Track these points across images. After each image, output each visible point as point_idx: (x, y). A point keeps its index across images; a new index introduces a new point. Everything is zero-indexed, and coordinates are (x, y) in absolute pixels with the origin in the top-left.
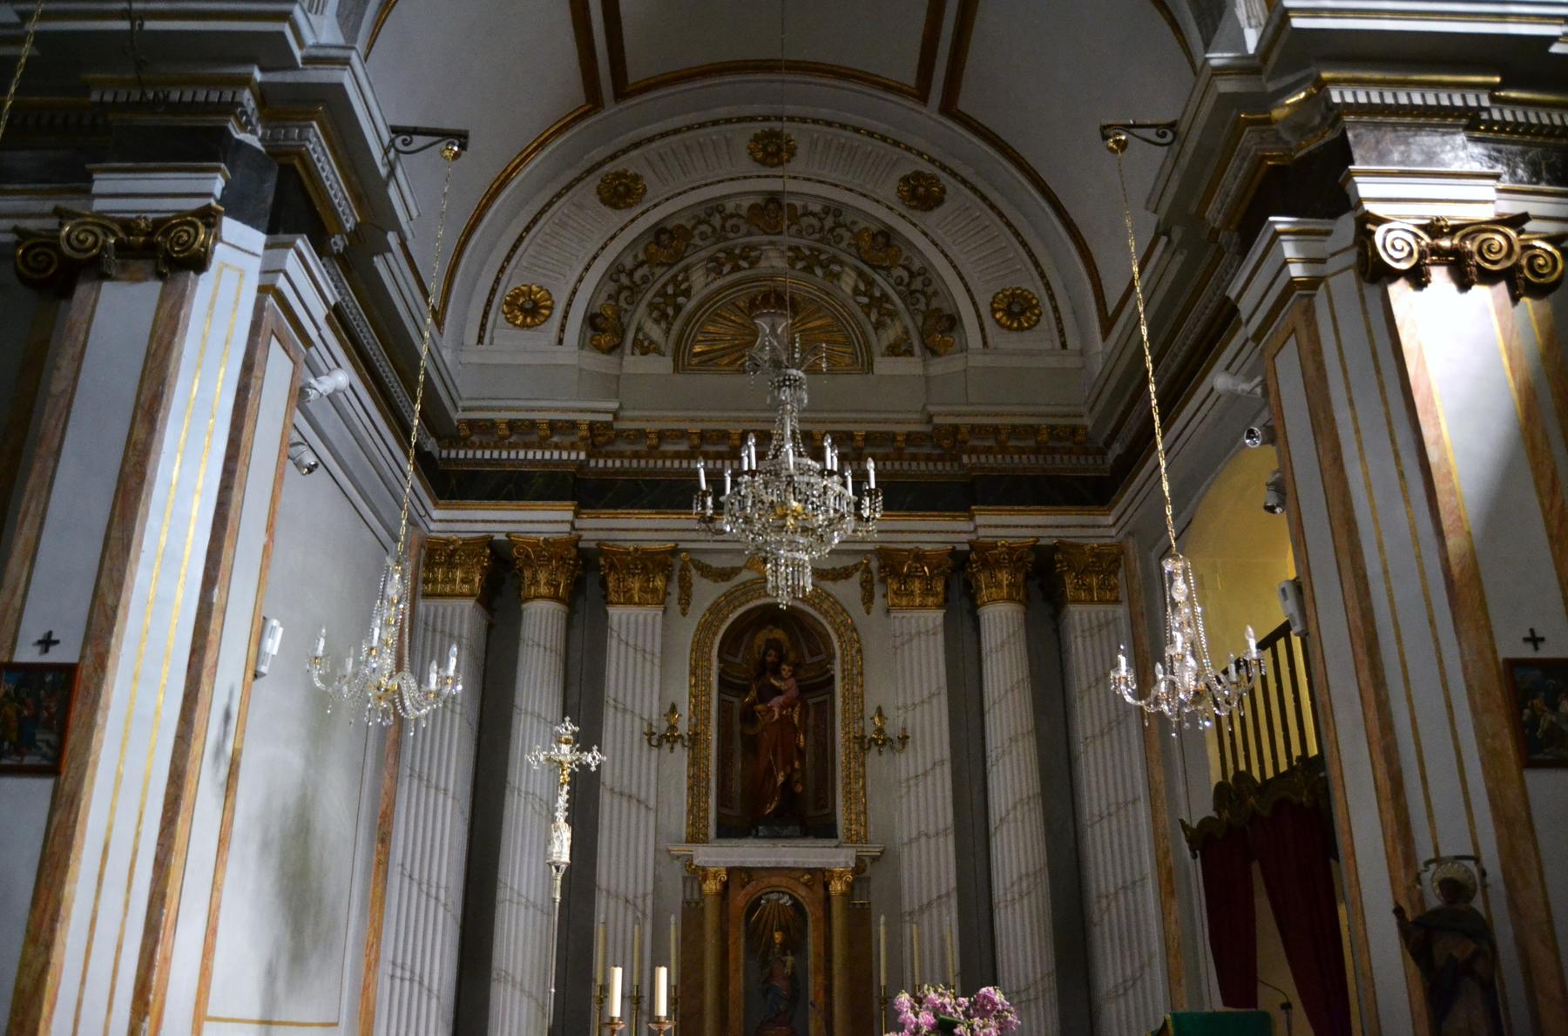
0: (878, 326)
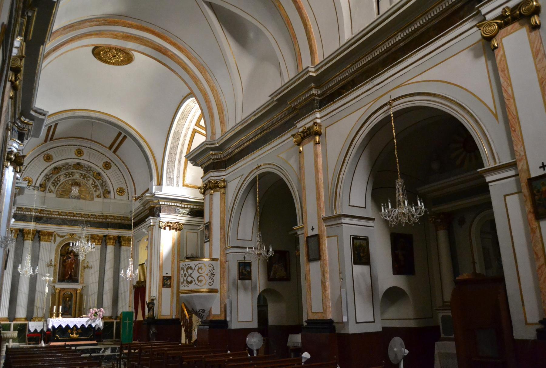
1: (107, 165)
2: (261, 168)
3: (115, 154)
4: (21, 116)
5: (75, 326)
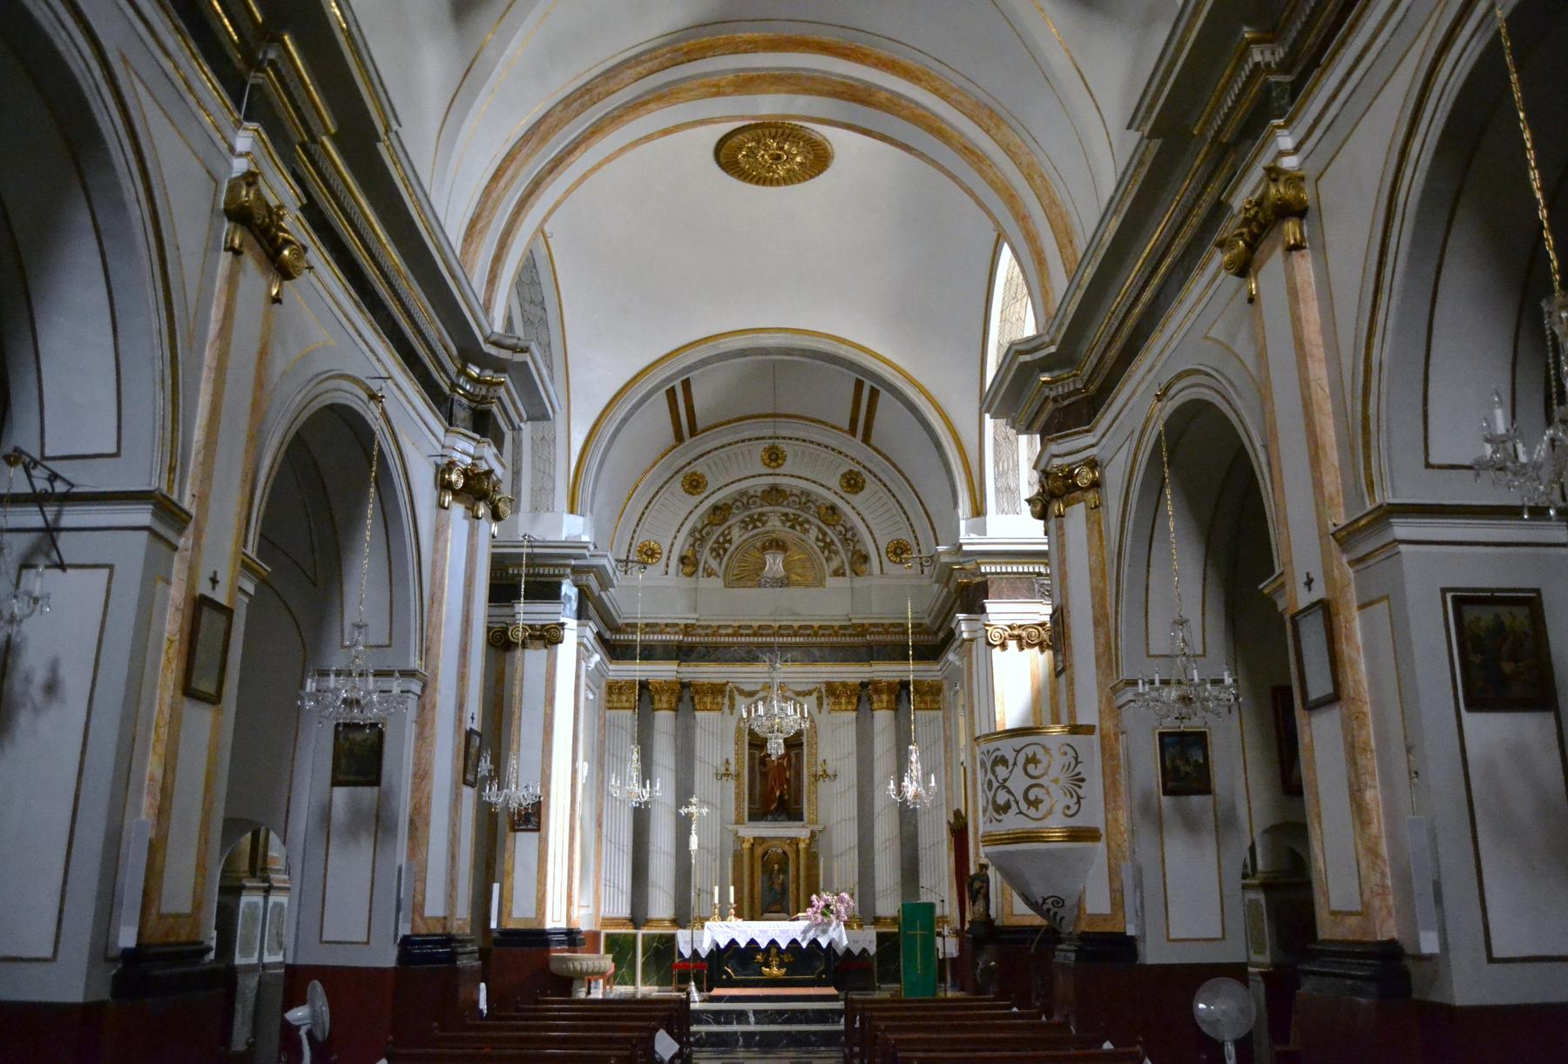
0: (828, 559)
1: (852, 482)
2: (1172, 392)
3: (870, 446)
4: (464, 366)
5: (773, 942)
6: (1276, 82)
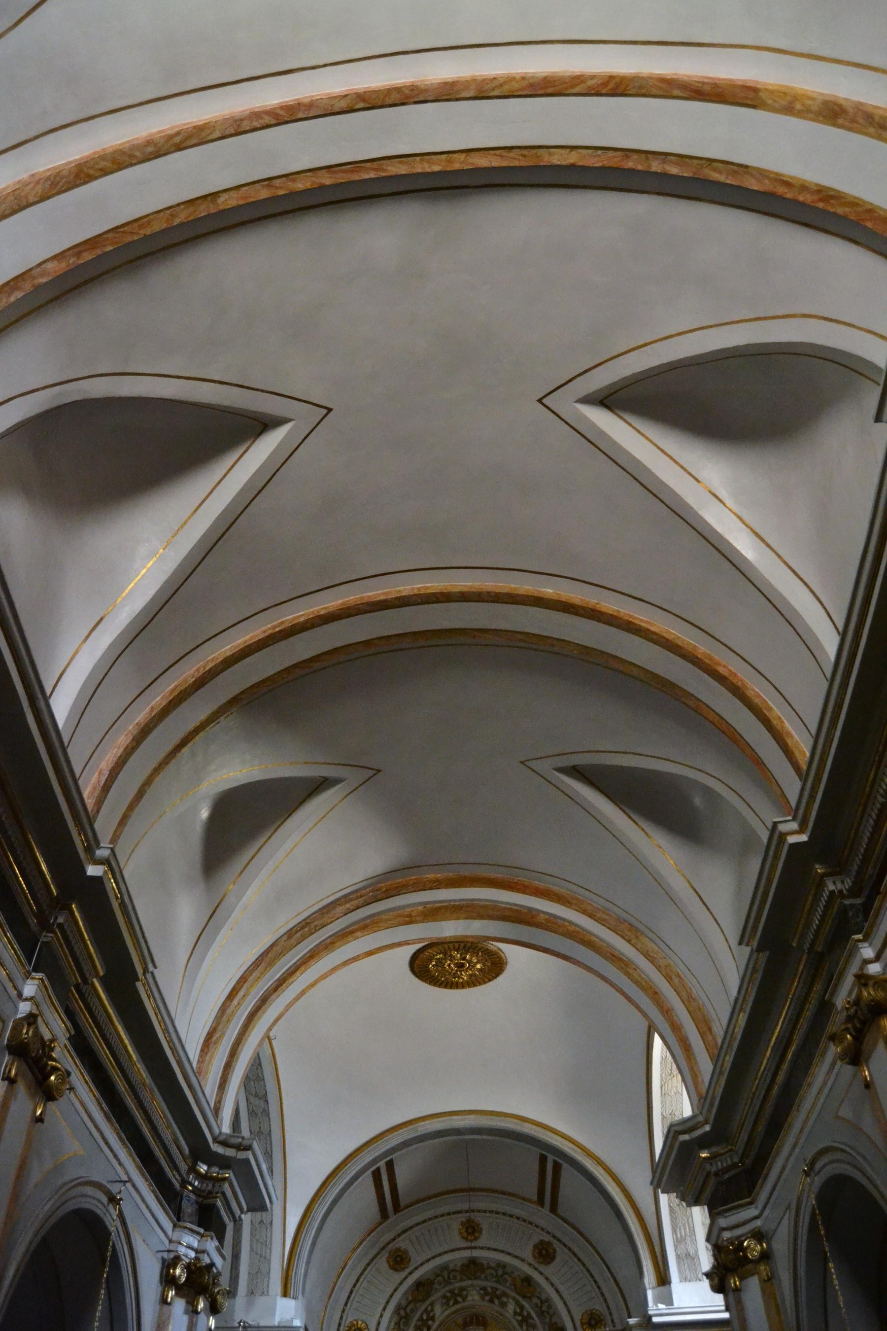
2: (818, 1166)
6: (850, 904)
